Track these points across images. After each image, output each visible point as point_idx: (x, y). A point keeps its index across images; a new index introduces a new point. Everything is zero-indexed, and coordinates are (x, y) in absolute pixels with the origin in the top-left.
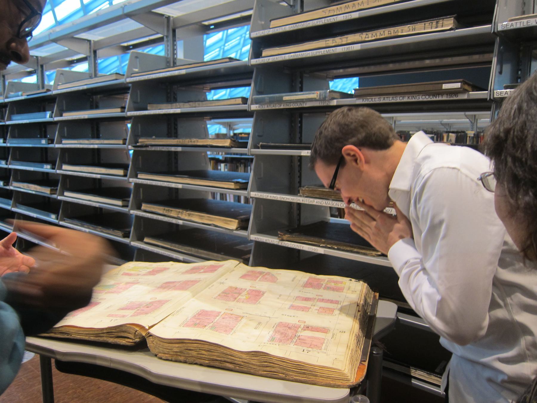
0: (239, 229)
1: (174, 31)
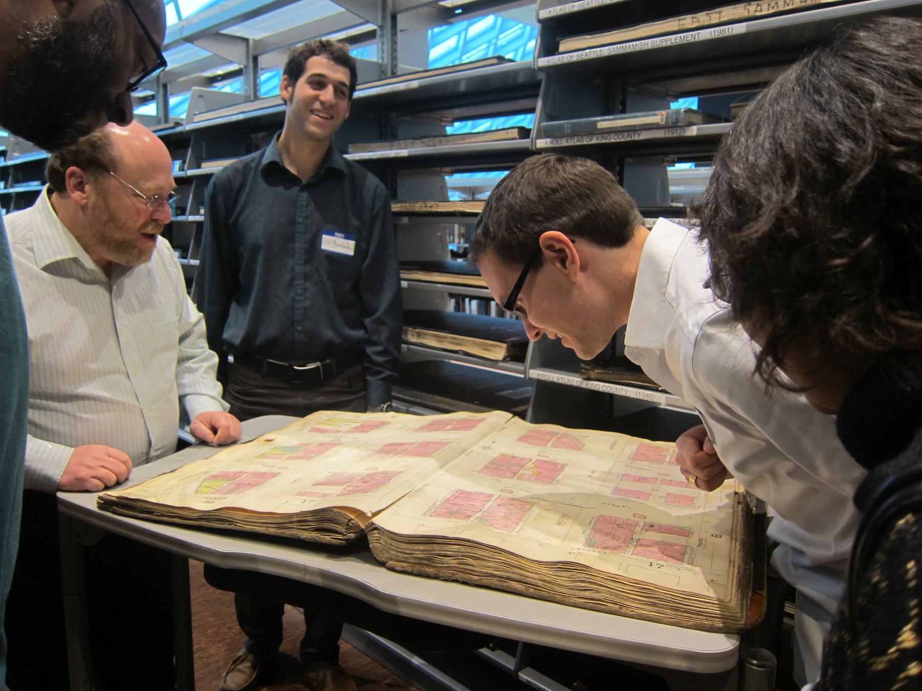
0: (508, 359)
1: (394, 18)
